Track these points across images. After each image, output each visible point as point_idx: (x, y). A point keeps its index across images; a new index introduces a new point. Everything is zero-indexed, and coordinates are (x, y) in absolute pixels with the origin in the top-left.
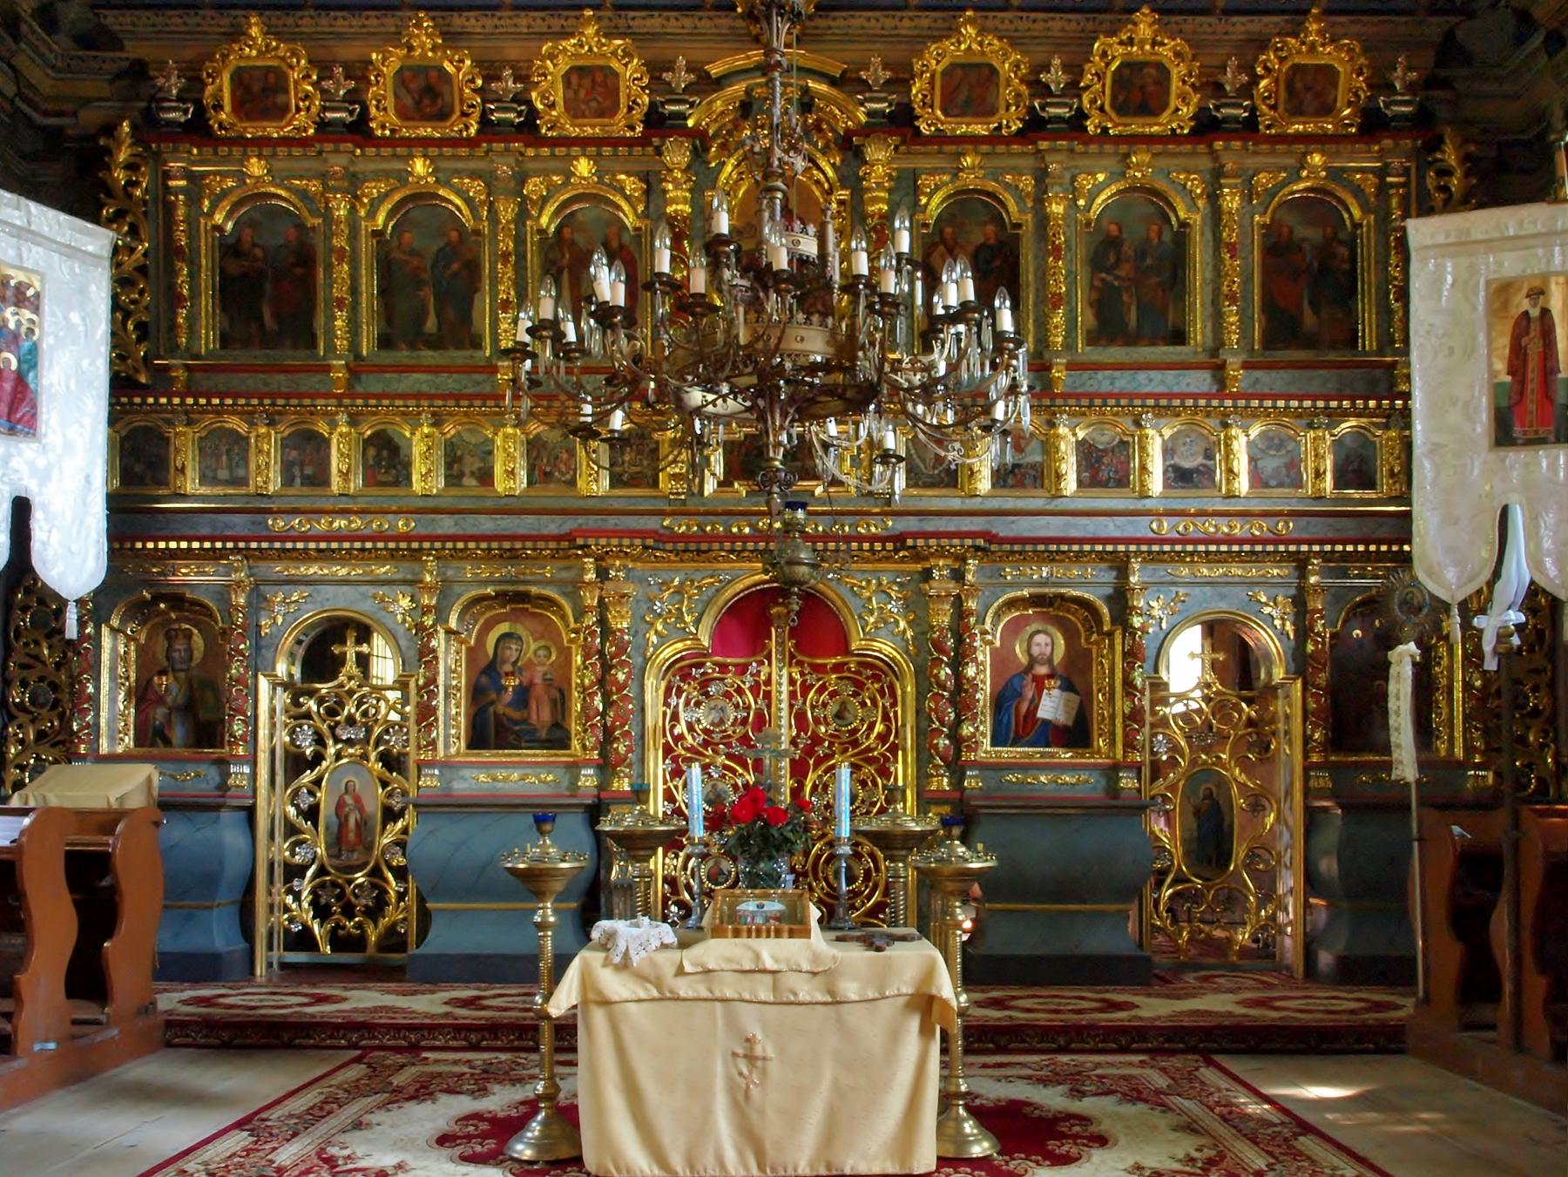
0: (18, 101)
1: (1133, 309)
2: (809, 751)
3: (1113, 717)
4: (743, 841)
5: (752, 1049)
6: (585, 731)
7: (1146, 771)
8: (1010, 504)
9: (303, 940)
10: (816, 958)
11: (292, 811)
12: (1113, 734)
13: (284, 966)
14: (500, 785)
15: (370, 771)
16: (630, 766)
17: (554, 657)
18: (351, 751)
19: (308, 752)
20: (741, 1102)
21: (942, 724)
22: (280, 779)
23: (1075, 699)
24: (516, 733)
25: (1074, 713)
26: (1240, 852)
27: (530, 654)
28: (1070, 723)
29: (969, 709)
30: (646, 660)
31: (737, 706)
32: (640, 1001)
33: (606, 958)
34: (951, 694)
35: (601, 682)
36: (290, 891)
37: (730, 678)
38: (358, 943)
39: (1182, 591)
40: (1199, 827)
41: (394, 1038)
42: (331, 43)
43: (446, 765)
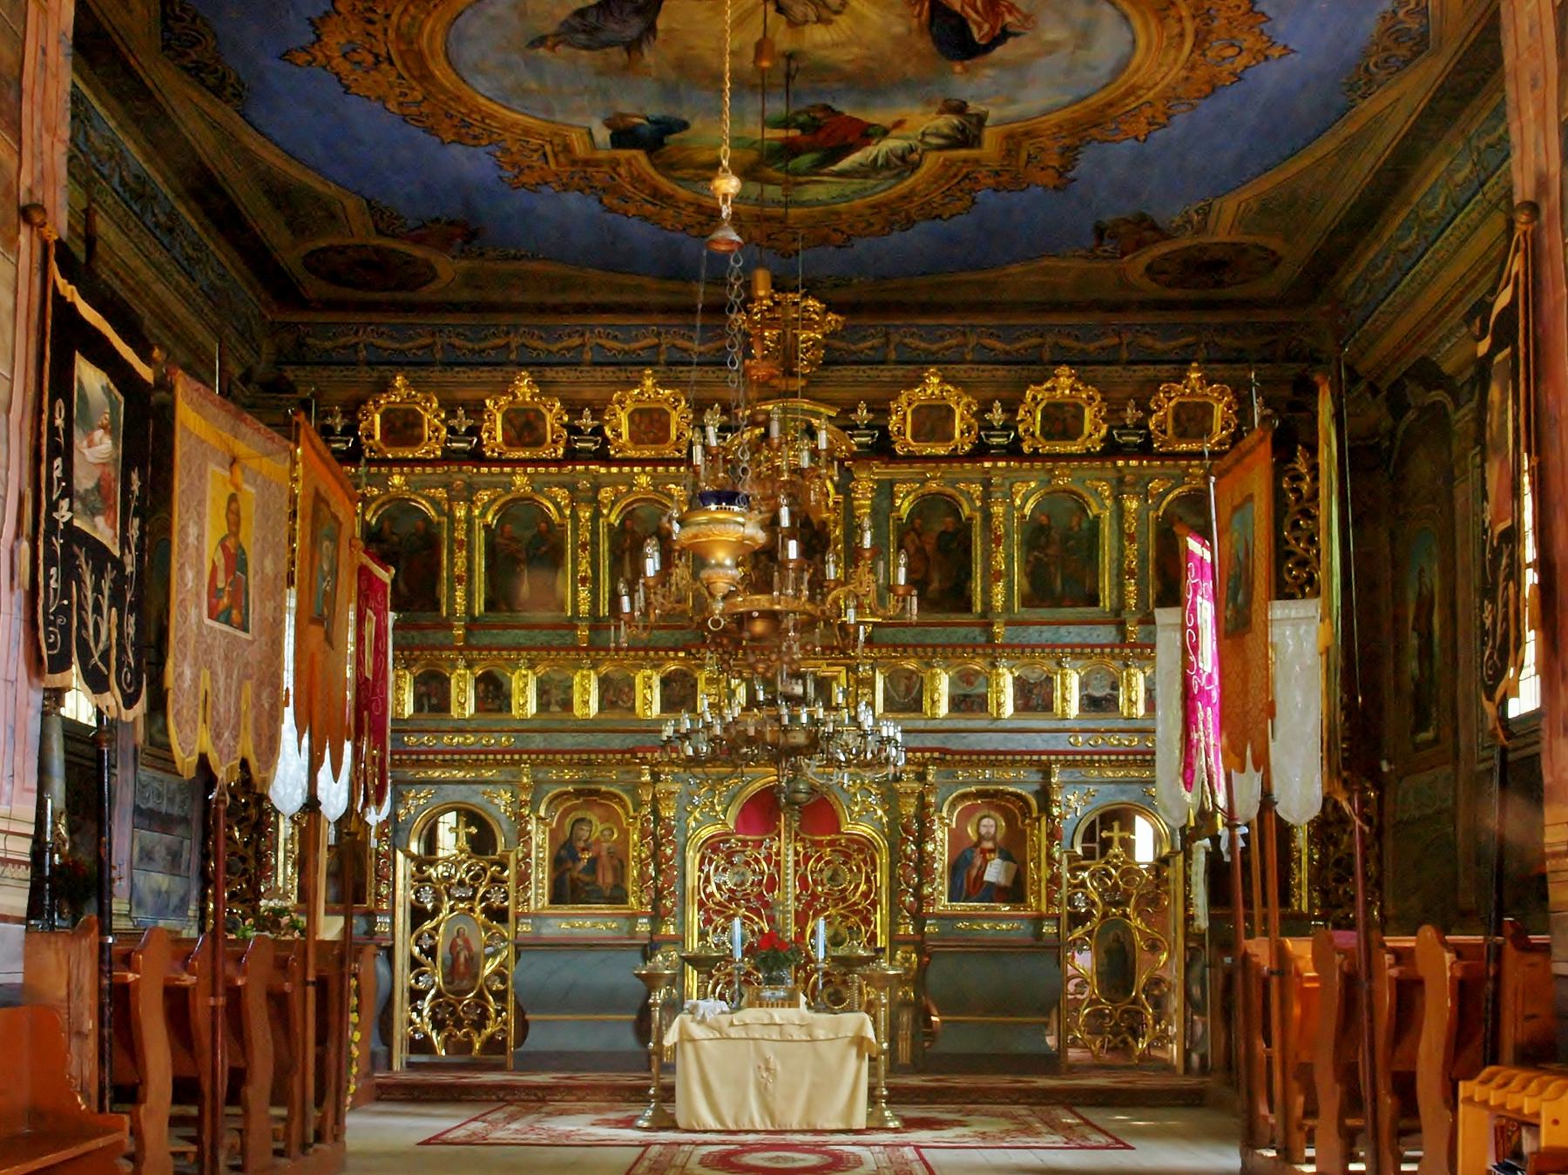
2: (809, 905)
10: (802, 1018)
11: (416, 950)
12: (1039, 892)
20: (762, 1091)
23: (1013, 866)
31: (754, 871)
35: (654, 855)
36: (415, 1009)
39: (1092, 788)
43: (536, 916)
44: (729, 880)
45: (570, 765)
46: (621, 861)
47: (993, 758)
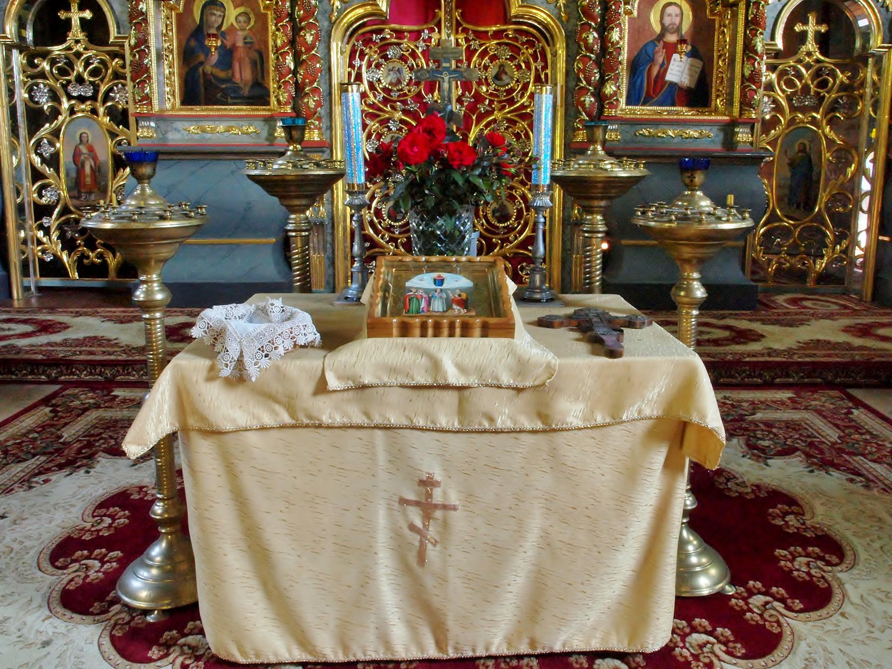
2: (472, 108)
3: (732, 80)
4: (415, 189)
5: (429, 495)
6: (279, 87)
7: (758, 126)
9: (53, 268)
10: (522, 366)
11: (37, 160)
12: (731, 94)
13: (40, 289)
14: (209, 136)
15: (100, 124)
16: (319, 119)
17: (252, 23)
18: (83, 106)
19: (45, 107)
20: (413, 563)
21: (589, 82)
22: (23, 131)
23: (699, 64)
24: (222, 90)
25: (697, 76)
26: (823, 197)
27: (232, 20)
29: (613, 70)
30: (332, 24)
31: (411, 68)
32: (263, 428)
33: (212, 368)
34: (597, 55)
35: (292, 42)
36: (41, 227)
37: (406, 43)
38: (101, 270)
40: (793, 175)
41: (91, 374)
43: (160, 118)
44: (384, 77)
45: (659, 72)
46: (261, 55)
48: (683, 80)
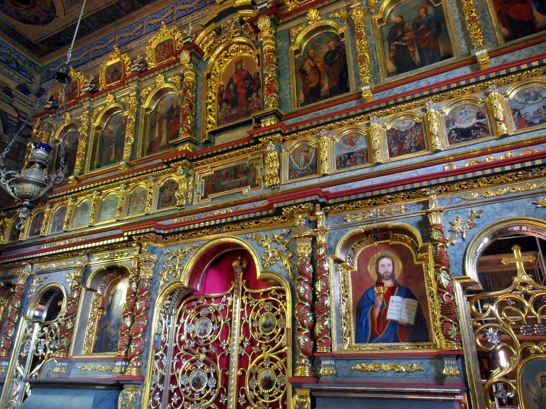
0: (20, 118)
1: (417, 53)
8: (348, 175)
23: (414, 303)
25: (414, 314)
28: (412, 323)
39: (475, 210)
42: (95, 69)
45: (380, 313)
47: (375, 196)
48: (402, 317)
